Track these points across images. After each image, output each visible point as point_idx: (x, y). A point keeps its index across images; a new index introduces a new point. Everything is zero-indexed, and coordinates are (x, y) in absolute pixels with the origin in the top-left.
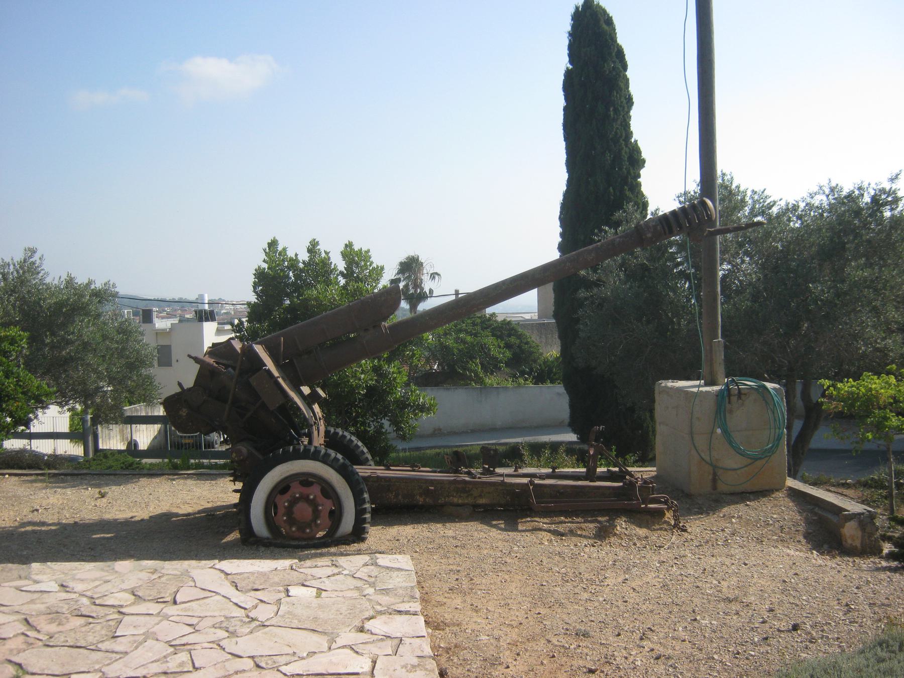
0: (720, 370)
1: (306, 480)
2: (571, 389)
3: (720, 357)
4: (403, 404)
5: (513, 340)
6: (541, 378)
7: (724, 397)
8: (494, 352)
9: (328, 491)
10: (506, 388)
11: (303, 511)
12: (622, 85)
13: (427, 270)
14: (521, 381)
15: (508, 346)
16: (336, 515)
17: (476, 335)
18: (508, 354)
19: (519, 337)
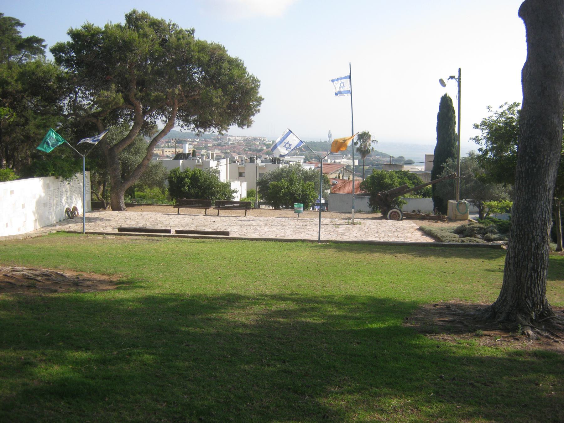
0: (459, 199)
1: (395, 212)
2: (435, 200)
3: (459, 197)
4: (400, 202)
5: (415, 181)
6: (425, 195)
7: (459, 203)
8: (408, 185)
9: (398, 213)
10: (412, 199)
11: (395, 216)
12: (455, 151)
13: (372, 139)
14: (418, 196)
15: (413, 183)
16: (399, 216)
17: (402, 179)
18: (413, 186)
19: (417, 180)
